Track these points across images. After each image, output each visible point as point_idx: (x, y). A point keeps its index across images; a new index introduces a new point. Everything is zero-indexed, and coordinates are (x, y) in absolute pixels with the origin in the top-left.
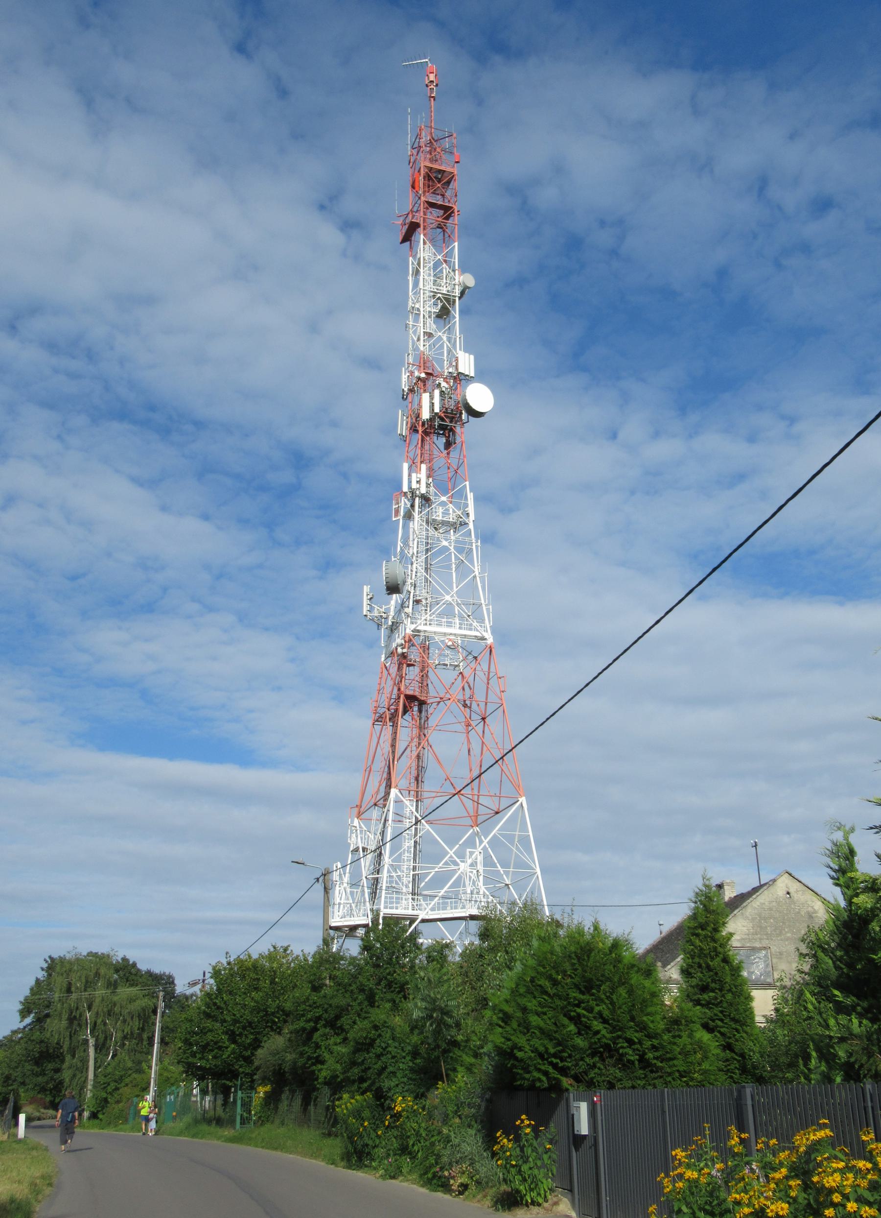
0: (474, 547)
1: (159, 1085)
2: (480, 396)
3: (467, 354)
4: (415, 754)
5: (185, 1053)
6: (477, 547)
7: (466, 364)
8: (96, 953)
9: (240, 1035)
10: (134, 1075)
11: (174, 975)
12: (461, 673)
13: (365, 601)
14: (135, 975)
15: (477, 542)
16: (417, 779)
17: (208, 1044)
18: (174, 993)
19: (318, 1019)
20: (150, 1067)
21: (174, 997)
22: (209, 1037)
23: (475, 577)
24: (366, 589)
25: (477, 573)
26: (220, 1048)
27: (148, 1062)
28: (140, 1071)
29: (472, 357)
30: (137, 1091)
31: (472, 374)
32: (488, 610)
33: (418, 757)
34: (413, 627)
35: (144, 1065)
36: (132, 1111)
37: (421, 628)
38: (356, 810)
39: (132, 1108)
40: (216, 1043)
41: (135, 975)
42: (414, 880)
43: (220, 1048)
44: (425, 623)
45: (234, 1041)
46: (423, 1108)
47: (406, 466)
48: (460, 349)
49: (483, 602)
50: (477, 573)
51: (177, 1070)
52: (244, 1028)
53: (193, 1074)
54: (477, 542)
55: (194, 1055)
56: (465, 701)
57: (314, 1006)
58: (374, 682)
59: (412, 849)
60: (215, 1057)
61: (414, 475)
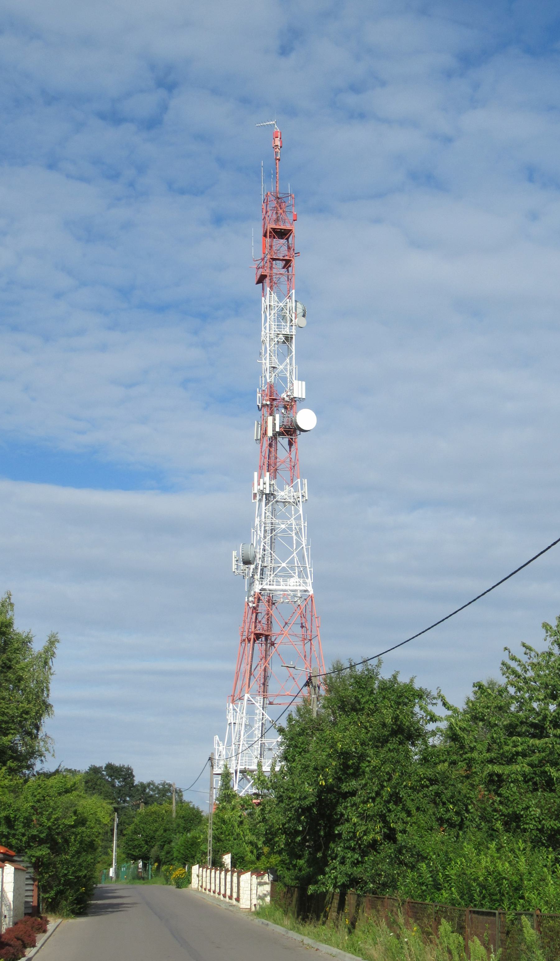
0: (303, 527)
1: (117, 862)
2: (306, 419)
3: (300, 382)
4: (263, 668)
5: (126, 848)
6: (304, 526)
7: (299, 389)
8: (70, 770)
9: (149, 842)
10: (104, 856)
11: (132, 767)
12: (299, 605)
13: (234, 562)
14: (100, 785)
15: (305, 523)
16: (264, 684)
17: (136, 846)
18: (133, 784)
19: (165, 842)
20: (112, 851)
21: (133, 786)
22: (136, 843)
23: (303, 547)
24: (234, 553)
25: (304, 545)
26: (141, 847)
27: (111, 848)
28: (107, 854)
29: (304, 383)
30: (105, 866)
31: (304, 397)
32: (310, 571)
33: (265, 670)
34: (261, 587)
35: (109, 850)
36: (103, 877)
37: (265, 587)
38: (231, 698)
39: (103, 876)
40: (139, 845)
41: (100, 785)
42: (261, 746)
43: (141, 847)
44: (268, 584)
45: (147, 845)
46: (340, 869)
47: (256, 474)
48: (296, 379)
49: (307, 565)
50: (304, 545)
51: (124, 856)
52: (151, 839)
53: (130, 858)
54: (305, 523)
55: (130, 850)
56: (302, 624)
57: (164, 837)
58: (237, 623)
59: (260, 728)
60: (139, 851)
61: (261, 480)
